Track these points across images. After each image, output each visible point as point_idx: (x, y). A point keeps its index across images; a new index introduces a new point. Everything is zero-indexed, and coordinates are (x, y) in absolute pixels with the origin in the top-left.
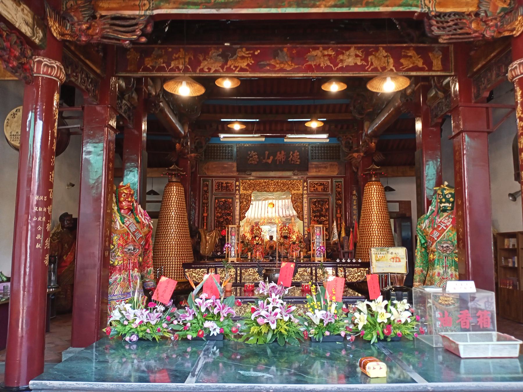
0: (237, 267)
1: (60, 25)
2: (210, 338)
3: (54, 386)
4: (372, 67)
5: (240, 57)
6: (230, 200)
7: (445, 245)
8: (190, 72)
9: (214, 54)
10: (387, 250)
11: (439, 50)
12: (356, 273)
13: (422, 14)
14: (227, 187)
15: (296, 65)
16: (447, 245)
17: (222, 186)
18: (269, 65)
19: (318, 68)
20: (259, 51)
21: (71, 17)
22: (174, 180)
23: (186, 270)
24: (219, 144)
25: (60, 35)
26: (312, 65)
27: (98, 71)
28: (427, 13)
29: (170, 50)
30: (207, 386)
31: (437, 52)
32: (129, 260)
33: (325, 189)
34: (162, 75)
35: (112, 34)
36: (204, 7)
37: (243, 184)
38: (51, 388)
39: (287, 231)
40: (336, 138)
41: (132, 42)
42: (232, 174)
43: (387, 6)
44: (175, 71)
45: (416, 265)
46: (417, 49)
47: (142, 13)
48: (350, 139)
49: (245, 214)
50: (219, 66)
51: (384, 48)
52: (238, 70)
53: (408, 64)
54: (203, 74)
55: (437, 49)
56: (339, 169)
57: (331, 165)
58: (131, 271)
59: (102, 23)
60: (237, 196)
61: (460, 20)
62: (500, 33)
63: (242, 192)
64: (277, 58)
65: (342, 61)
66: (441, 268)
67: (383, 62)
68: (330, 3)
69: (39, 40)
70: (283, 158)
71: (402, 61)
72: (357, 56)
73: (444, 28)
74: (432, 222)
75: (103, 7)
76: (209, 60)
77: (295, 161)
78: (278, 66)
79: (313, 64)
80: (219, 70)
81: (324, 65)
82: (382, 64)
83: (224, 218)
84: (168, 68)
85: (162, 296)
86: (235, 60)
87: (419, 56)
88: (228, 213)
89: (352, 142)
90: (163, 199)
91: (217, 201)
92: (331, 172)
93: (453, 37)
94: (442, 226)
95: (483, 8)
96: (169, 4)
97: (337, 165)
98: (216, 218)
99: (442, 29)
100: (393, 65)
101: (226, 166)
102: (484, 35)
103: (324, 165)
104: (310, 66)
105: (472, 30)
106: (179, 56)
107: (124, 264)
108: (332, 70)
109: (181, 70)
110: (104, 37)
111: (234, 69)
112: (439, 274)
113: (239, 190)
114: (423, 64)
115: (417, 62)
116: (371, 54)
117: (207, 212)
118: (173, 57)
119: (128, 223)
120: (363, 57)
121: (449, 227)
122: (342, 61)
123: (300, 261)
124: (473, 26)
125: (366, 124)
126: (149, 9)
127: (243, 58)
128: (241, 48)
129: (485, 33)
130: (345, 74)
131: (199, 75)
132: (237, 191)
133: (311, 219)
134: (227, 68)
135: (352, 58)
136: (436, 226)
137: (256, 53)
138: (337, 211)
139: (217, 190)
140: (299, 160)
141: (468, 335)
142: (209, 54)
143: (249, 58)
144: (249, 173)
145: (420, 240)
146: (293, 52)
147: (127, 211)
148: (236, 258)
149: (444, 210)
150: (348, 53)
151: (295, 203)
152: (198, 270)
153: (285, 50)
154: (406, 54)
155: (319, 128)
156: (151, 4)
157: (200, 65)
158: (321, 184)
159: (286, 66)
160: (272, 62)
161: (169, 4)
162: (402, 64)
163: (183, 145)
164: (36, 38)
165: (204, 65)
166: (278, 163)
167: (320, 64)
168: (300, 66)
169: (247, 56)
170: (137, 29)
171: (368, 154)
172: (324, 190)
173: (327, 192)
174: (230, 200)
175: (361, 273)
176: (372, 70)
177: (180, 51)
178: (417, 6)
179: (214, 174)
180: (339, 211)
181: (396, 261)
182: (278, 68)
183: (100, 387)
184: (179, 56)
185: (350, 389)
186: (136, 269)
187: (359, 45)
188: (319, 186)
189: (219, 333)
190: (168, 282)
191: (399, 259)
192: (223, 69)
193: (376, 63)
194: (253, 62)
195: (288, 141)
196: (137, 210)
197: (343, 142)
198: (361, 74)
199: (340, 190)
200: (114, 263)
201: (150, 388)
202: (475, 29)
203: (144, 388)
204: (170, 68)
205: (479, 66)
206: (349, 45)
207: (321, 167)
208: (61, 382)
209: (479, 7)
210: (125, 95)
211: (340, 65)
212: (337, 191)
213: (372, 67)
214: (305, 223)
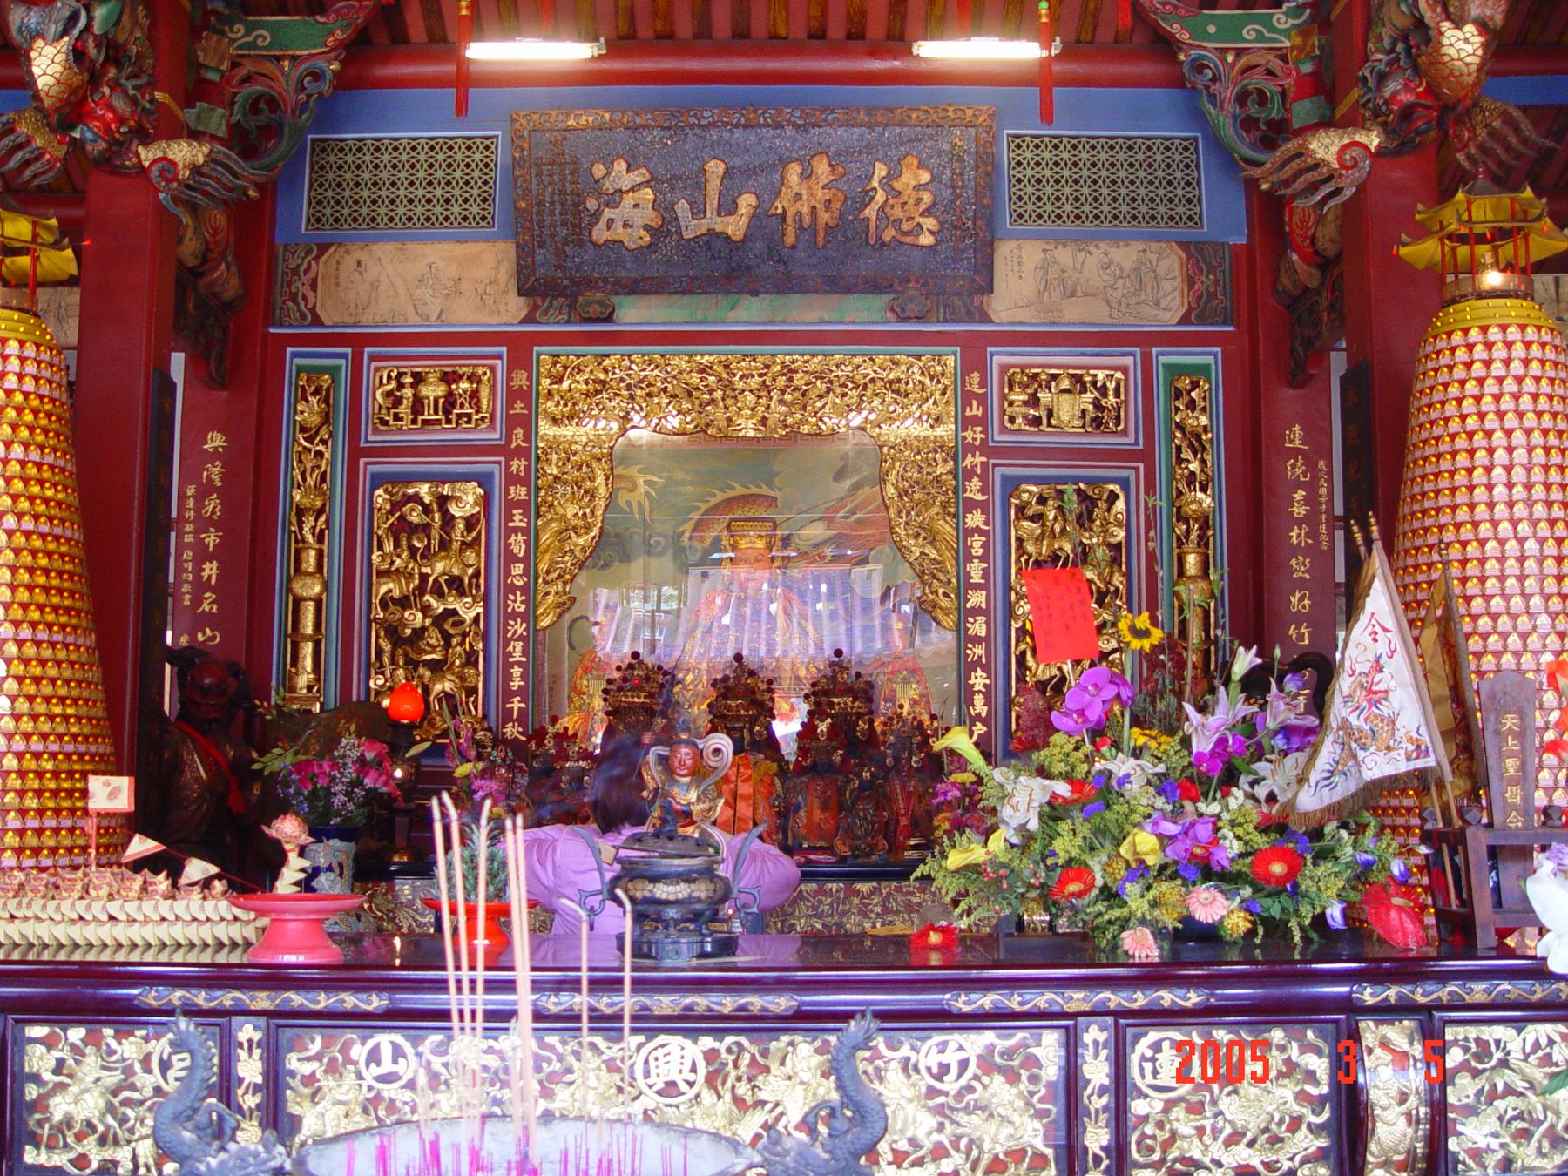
140: (929, 223)
180: (1192, 561)
199: (1204, 420)
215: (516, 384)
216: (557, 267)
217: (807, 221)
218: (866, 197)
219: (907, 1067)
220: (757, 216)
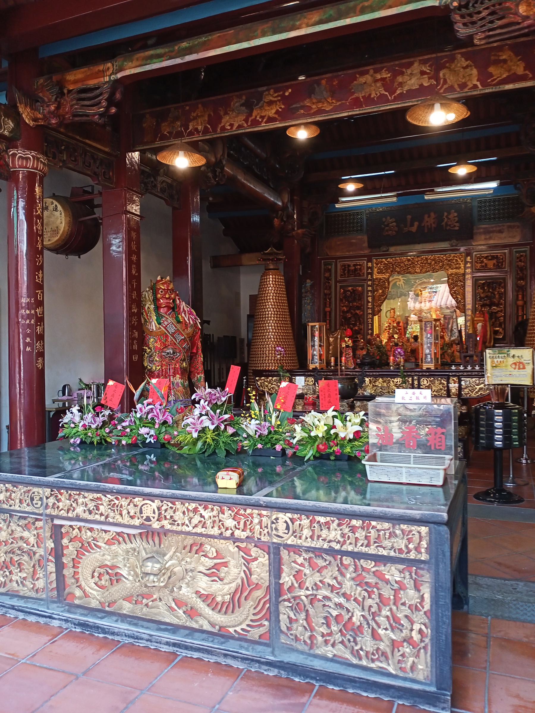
1: (32, 109)
5: (267, 103)
6: (360, 289)
8: (210, 132)
9: (237, 104)
10: (508, 351)
12: (477, 385)
14: (356, 270)
15: (338, 101)
19: (369, 101)
20: (290, 90)
21: (41, 98)
22: (271, 267)
23: (257, 378)
25: (33, 121)
26: (359, 98)
27: (107, 150)
29: (187, 108)
32: (170, 365)
35: (81, 111)
37: (377, 264)
40: (512, 186)
41: (101, 115)
42: (362, 252)
43: (390, 7)
44: (194, 135)
47: (107, 79)
51: (463, 55)
52: (264, 121)
53: (500, 72)
54: (225, 133)
57: (509, 227)
58: (171, 377)
64: (313, 95)
65: (401, 84)
67: (462, 77)
68: (313, 20)
69: (8, 131)
70: (434, 223)
71: (491, 69)
72: (423, 73)
73: (473, 23)
79: (360, 95)
80: (243, 124)
81: (376, 94)
82: (460, 80)
83: (351, 313)
84: (186, 133)
85: (111, 400)
86: (261, 108)
87: (519, 58)
88: (357, 306)
90: (259, 291)
92: (510, 237)
96: (132, 62)
97: (518, 227)
98: (341, 314)
99: (470, 25)
100: (476, 78)
101: (354, 241)
103: (498, 229)
104: (357, 99)
105: (519, 16)
106: (197, 114)
107: (162, 370)
108: (388, 101)
109: (200, 132)
110: (75, 116)
113: (372, 274)
115: (515, 68)
116: (444, 67)
117: (330, 305)
118: (191, 117)
119: (166, 323)
126: (113, 73)
128: (268, 90)
131: (220, 135)
135: (416, 78)
137: (287, 94)
140: (457, 224)
141: (412, 457)
144: (385, 249)
146: (334, 83)
147: (166, 309)
148: (433, 364)
150: (409, 71)
151: (453, 288)
152: (270, 378)
153: (324, 82)
154: (497, 58)
155: (470, 175)
157: (220, 123)
158: (493, 258)
159: (326, 105)
160: (307, 103)
161: (132, 62)
162: (491, 75)
163: (282, 220)
164: (4, 130)
165: (226, 121)
166: (426, 231)
167: (370, 95)
168: (344, 102)
169: (276, 99)
170: (102, 100)
173: (503, 268)
174: (360, 289)
177: (198, 108)
179: (339, 254)
180: (520, 296)
181: (519, 369)
182: (315, 110)
185: (183, 495)
186: (178, 376)
188: (490, 260)
190: (116, 386)
192: (247, 123)
194: (283, 107)
195: (431, 198)
196: (180, 308)
199: (523, 264)
200: (152, 368)
201: (20, 479)
202: (524, 14)
203: (15, 478)
206: (412, 60)
207: (493, 232)
210: (159, 170)
211: (398, 92)
213: (445, 86)
215: (369, 266)
216: (228, 453)
217: (429, 227)
218: (443, 220)
219: (393, 381)
220: (419, 226)
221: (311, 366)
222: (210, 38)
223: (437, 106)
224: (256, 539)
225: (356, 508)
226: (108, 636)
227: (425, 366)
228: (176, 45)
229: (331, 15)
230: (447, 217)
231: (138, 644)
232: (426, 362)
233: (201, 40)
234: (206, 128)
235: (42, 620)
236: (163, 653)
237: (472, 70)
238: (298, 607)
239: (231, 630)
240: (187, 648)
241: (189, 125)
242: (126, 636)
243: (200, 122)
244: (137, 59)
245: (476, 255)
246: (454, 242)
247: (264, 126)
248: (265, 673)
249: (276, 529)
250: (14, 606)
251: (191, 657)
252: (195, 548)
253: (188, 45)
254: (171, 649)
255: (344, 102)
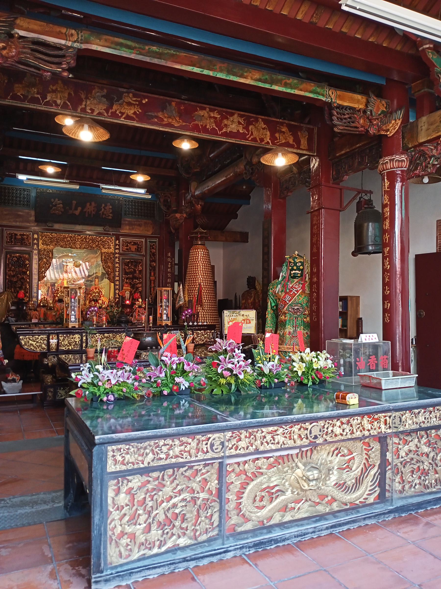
0: (82, 332)
2: (181, 393)
3: (120, 438)
4: (252, 137)
5: (126, 103)
6: (27, 256)
7: (296, 308)
8: (70, 109)
9: (98, 94)
11: (306, 130)
13: (325, 103)
15: (184, 121)
16: (298, 307)
17: (15, 238)
18: (157, 117)
24: (7, 185)
28: (330, 103)
30: (249, 422)
31: (304, 132)
33: (138, 250)
34: (35, 107)
36: (138, 52)
38: (117, 440)
39: (97, 294)
41: (54, 74)
44: (52, 106)
45: (266, 326)
46: (289, 126)
47: (69, 44)
48: (169, 197)
49: (45, 273)
50: (103, 108)
51: (263, 120)
55: (304, 129)
56: (153, 228)
59: (21, 45)
60: (35, 252)
61: (353, 114)
62: (379, 131)
63: (41, 246)
64: (165, 111)
66: (292, 328)
70: (94, 211)
71: (277, 135)
73: (341, 119)
74: (285, 286)
75: (22, 26)
76: (92, 99)
77: (107, 215)
78: (165, 120)
80: (103, 112)
86: (121, 105)
88: (23, 272)
89: (171, 201)
91: (8, 256)
93: (346, 128)
94: (294, 291)
95: (370, 108)
102: (368, 131)
104: (197, 125)
106: (57, 89)
108: (217, 134)
109: (59, 105)
111: (120, 115)
112: (290, 332)
114: (293, 142)
116: (252, 124)
120: (245, 125)
121: (300, 292)
122: (226, 126)
123: (102, 326)
124: (361, 121)
125: (193, 185)
127: (129, 104)
128: (128, 93)
129: (369, 129)
130: (229, 139)
132: (36, 246)
133: (123, 281)
134: (112, 113)
135: (235, 125)
136: (288, 291)
137: (144, 102)
138: (150, 273)
139: (9, 242)
140: (111, 215)
142: (92, 93)
143: (136, 106)
144: (50, 225)
145: (271, 303)
146: (181, 108)
149: (294, 277)
150: (231, 119)
152: (37, 336)
156: (80, 36)
158: (135, 244)
159: (174, 121)
160: (160, 115)
161: (100, 40)
166: (87, 216)
167: (206, 126)
169: (134, 103)
171: (192, 216)
172: (138, 250)
174: (27, 256)
175: (208, 335)
176: (252, 140)
177: (58, 83)
178: (323, 95)
180: (152, 273)
181: (247, 323)
182: (166, 123)
183: (163, 433)
184: (57, 89)
185: (345, 413)
187: (242, 113)
188: (132, 245)
189: (187, 387)
190: (131, 342)
191: (249, 320)
192: (107, 113)
193: (255, 134)
194: (140, 111)
195: (106, 192)
197: (162, 200)
198: (242, 142)
204: (45, 101)
205: (343, 152)
206: (233, 111)
207: (135, 225)
208: (127, 434)
209: (366, 106)
211: (224, 130)
212: (151, 252)
213: (252, 137)
214: (117, 285)
217: (90, 213)
220: (82, 211)
221: (71, 325)
222: (178, 54)
223: (280, 154)
224: (384, 433)
225: (307, 415)
226: (278, 544)
227: (71, 325)
228: (147, 45)
229: (267, 79)
230: (103, 207)
231: (304, 539)
232: (71, 322)
233: (169, 52)
234: (65, 103)
235: (214, 559)
236: (323, 537)
237: (267, 131)
238: (397, 471)
239: (357, 502)
240: (340, 525)
241: (46, 96)
242: (295, 537)
243: (59, 96)
244: (106, 40)
245: (122, 240)
246: (107, 228)
247: (122, 121)
248: (387, 519)
249: (395, 423)
250: (184, 558)
251: (343, 531)
252: (336, 452)
253: (157, 50)
254: (328, 532)
255: (188, 124)
